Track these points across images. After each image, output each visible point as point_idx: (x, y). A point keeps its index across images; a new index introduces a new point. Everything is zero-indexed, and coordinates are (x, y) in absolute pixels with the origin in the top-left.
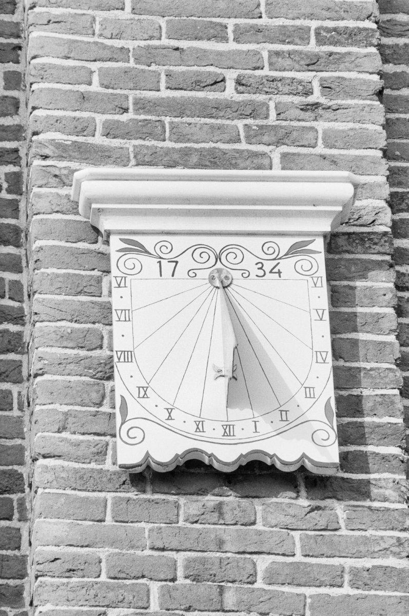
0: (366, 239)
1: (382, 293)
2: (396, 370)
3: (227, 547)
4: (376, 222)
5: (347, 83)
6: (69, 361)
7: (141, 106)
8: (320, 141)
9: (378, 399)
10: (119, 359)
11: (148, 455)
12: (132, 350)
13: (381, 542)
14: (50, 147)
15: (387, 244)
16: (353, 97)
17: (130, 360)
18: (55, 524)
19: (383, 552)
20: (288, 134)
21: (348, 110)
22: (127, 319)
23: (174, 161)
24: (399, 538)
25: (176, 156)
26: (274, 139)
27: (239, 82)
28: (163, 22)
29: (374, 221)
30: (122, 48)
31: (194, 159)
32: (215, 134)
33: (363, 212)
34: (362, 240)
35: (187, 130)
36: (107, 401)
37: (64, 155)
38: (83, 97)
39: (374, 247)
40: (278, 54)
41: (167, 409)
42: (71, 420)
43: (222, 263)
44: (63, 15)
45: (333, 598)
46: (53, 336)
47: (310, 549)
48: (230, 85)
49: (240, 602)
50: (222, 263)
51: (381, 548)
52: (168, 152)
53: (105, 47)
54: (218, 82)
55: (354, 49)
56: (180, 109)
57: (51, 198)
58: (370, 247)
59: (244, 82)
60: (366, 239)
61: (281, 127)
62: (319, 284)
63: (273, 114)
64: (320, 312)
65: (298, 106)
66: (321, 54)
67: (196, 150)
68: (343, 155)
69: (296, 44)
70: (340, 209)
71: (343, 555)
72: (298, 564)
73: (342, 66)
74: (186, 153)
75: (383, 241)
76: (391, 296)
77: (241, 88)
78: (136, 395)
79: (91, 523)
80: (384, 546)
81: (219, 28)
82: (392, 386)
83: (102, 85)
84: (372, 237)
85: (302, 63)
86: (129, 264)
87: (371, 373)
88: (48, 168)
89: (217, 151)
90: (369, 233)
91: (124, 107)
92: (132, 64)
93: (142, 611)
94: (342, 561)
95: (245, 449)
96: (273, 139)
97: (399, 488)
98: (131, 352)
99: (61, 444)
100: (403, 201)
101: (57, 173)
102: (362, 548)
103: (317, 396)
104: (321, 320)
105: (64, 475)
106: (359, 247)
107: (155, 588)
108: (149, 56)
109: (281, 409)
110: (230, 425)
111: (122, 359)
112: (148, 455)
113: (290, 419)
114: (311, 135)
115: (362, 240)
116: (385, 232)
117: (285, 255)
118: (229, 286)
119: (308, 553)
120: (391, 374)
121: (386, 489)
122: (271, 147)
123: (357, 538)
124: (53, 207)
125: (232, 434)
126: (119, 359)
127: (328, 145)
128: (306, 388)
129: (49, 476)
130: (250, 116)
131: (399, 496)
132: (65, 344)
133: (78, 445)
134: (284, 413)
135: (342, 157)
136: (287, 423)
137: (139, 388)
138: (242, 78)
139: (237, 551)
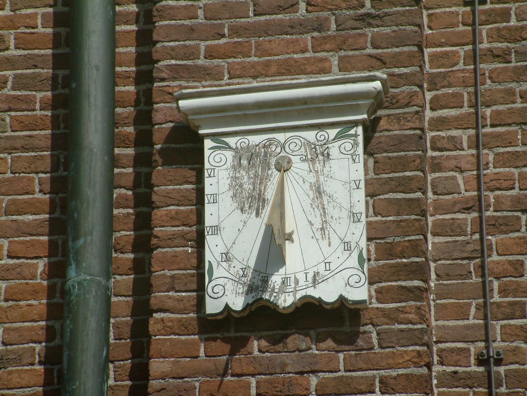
1: (413, 159)
2: (295, 296)
4: (410, 104)
6: (176, 236)
7: (235, 31)
8: (369, 45)
9: (407, 244)
10: (208, 233)
11: (227, 306)
14: (166, 71)
18: (162, 362)
26: (334, 46)
31: (273, 69)
33: (400, 97)
34: (399, 119)
35: (267, 46)
36: (58, 337)
37: (176, 76)
38: (192, 29)
39: (407, 124)
41: (242, 269)
42: (176, 281)
46: (164, 218)
50: (285, 151)
51: (404, 360)
52: (253, 65)
56: (266, 30)
61: (340, 36)
62: (357, 160)
63: (333, 26)
68: (386, 53)
72: (342, 376)
74: (267, 64)
75: (414, 118)
77: (310, 8)
79: (189, 359)
83: (206, 18)
86: (217, 159)
87: (402, 224)
88: (164, 88)
89: (291, 60)
90: (404, 113)
97: (420, 312)
98: (217, 226)
99: (168, 300)
100: (445, 79)
102: (391, 361)
103: (352, 249)
104: (358, 188)
105: (169, 324)
109: (325, 261)
110: (287, 278)
111: (210, 233)
112: (227, 306)
113: (332, 269)
114: (362, 40)
115: (399, 119)
117: (333, 140)
118: (288, 170)
119: (349, 368)
120: (417, 224)
121: (410, 313)
122: (331, 53)
123: (387, 354)
124: (167, 118)
125: (288, 285)
126: (208, 233)
127: (375, 47)
129: (159, 326)
130: (314, 30)
131: (420, 318)
132: (174, 223)
133: (181, 299)
134: (327, 264)
136: (330, 271)
137: (222, 254)
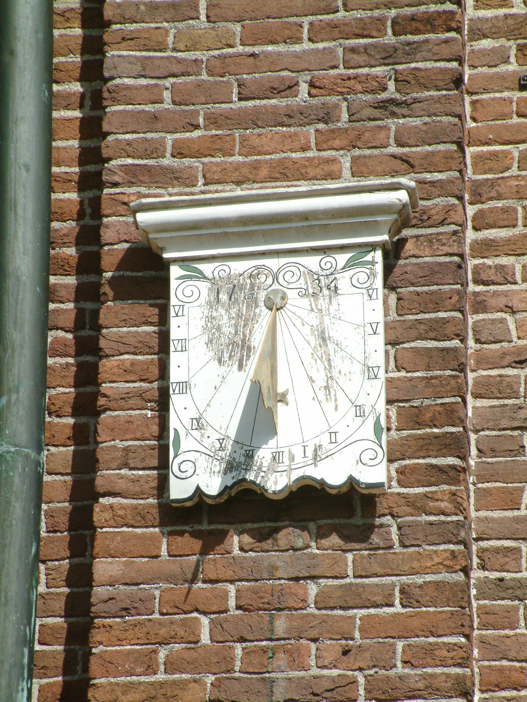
0: (434, 241)
3: (280, 573)
4: (446, 222)
5: (423, 74)
6: (131, 395)
7: (213, 121)
8: (392, 141)
10: (174, 391)
11: (198, 489)
12: (187, 380)
13: (434, 556)
14: (120, 173)
15: (456, 244)
16: (428, 89)
17: (184, 392)
18: (111, 563)
19: (436, 567)
20: (359, 137)
21: (422, 104)
22: (184, 349)
23: (244, 176)
24: (453, 551)
25: (245, 171)
27: (312, 85)
28: (237, 28)
29: (443, 221)
30: (195, 61)
32: (286, 143)
33: (433, 212)
35: (256, 141)
37: (133, 180)
38: (155, 117)
40: (353, 50)
41: (219, 440)
42: (131, 455)
43: (279, 283)
44: (138, 31)
45: (384, 618)
46: (116, 370)
47: (364, 569)
48: (304, 88)
49: (289, 630)
50: (279, 283)
51: (434, 563)
52: (237, 167)
53: (179, 61)
54: (291, 87)
55: (432, 36)
56: (254, 120)
57: (118, 227)
58: (438, 248)
59: (317, 84)
60: (434, 241)
62: (374, 296)
64: (374, 326)
65: (372, 104)
66: (397, 45)
67: (266, 162)
69: (373, 37)
70: (395, 216)
71: (395, 573)
73: (418, 56)
74: (255, 166)
76: (457, 299)
77: (314, 91)
78: (189, 427)
80: (437, 560)
81: (294, 28)
82: (453, 394)
83: (174, 103)
84: (441, 237)
85: (377, 56)
87: (433, 381)
88: (117, 196)
90: (438, 234)
91: (195, 123)
92: (204, 76)
93: (192, 646)
94: (394, 578)
95: (295, 476)
96: (344, 142)
98: (186, 382)
100: (493, 188)
101: (126, 200)
102: (416, 564)
103: (366, 415)
104: (375, 333)
106: (427, 249)
107: (205, 621)
108: (222, 67)
111: (177, 391)
112: (198, 489)
113: (339, 440)
114: (383, 134)
115: (430, 241)
116: (454, 231)
117: (342, 269)
118: (282, 308)
121: (442, 501)
122: (342, 152)
123: (411, 554)
124: (121, 236)
126: (174, 391)
127: (400, 144)
128: (356, 406)
129: (107, 515)
132: (128, 378)
133: (136, 480)
134: (333, 435)
135: (413, 156)
137: (192, 419)
138: (316, 80)
139: (294, 576)
